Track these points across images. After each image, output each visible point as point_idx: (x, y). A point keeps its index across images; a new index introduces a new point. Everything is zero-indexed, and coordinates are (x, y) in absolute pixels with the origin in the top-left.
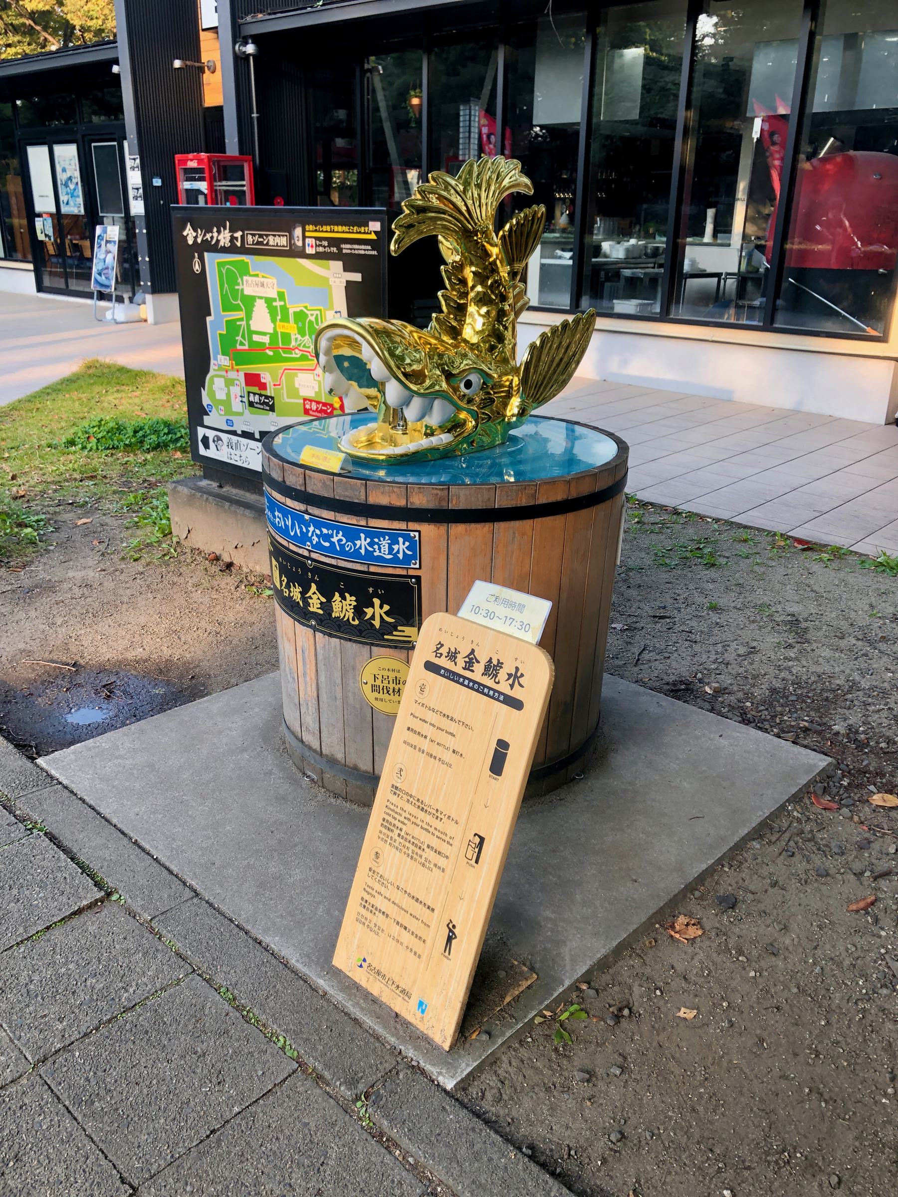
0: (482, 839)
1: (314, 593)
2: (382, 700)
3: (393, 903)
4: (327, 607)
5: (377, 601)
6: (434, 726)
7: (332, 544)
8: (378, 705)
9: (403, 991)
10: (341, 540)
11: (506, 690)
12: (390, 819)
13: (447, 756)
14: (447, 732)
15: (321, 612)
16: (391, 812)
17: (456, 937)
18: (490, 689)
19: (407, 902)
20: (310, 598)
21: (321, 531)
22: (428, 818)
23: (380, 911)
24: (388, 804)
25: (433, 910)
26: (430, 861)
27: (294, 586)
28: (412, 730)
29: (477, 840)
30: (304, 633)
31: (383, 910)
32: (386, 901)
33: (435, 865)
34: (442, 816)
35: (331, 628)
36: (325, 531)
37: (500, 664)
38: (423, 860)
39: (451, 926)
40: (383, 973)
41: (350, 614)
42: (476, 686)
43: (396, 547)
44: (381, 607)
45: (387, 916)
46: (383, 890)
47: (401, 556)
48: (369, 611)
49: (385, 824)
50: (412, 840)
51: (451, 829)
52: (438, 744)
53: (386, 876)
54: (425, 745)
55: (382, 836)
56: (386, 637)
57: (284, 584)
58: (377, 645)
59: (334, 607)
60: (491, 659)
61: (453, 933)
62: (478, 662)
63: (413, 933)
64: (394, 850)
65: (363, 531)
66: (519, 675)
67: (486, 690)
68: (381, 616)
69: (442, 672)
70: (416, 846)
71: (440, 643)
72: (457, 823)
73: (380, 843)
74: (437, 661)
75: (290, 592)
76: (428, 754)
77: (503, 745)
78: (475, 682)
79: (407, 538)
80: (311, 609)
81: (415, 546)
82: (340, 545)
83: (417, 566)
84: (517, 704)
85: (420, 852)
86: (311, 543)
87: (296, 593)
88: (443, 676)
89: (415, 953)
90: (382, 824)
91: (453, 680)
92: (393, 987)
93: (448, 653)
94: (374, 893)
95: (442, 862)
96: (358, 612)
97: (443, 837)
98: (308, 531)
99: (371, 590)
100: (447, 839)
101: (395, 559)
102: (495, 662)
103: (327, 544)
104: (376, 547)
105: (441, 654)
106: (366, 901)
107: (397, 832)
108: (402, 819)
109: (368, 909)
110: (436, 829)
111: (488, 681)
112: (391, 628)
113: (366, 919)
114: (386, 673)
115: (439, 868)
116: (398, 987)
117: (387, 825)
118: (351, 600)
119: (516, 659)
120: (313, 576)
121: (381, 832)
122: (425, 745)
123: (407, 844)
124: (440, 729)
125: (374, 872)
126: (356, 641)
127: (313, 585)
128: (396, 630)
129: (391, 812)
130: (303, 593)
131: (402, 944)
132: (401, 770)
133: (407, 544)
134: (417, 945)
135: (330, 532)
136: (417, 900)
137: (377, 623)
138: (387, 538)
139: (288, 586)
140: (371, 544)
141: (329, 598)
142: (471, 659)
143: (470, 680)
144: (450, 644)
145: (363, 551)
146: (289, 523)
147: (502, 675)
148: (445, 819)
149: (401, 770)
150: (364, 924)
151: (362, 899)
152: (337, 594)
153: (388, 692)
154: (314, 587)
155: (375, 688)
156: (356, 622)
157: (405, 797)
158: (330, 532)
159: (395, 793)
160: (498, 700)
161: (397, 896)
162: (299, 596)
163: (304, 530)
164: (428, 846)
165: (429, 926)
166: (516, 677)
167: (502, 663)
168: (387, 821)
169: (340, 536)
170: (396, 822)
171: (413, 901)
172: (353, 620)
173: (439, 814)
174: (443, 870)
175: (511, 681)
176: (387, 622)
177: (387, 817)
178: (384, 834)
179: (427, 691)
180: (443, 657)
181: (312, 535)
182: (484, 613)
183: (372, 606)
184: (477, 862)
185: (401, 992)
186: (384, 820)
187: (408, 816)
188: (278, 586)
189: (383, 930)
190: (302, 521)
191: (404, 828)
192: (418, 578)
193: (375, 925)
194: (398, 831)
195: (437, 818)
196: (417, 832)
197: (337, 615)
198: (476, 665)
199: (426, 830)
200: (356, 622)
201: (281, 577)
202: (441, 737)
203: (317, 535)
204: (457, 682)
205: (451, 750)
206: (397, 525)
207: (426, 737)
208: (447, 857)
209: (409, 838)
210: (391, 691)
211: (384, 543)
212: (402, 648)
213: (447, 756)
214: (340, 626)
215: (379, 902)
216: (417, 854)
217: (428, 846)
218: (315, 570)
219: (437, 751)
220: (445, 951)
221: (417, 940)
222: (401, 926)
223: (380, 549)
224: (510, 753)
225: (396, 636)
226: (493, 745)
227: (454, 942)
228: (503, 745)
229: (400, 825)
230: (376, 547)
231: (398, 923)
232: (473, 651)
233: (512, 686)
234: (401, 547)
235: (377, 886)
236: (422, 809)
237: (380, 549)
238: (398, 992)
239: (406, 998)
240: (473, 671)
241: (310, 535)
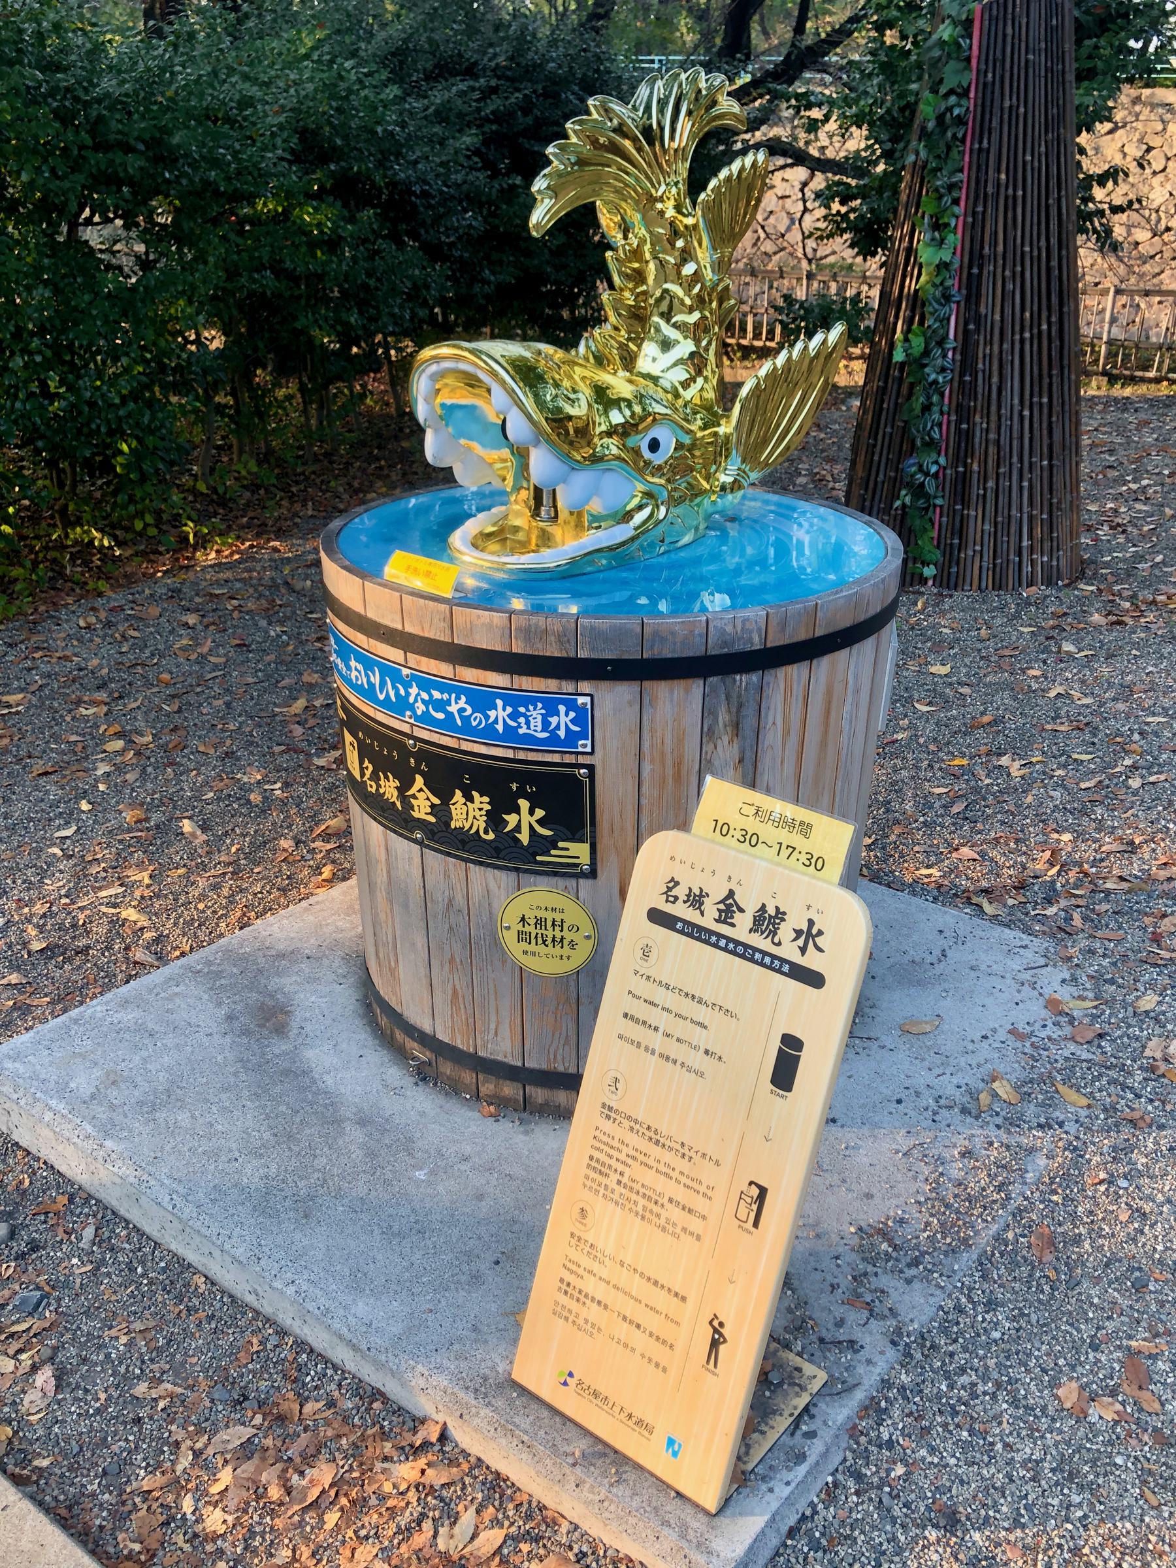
0: (763, 1191)
1: (421, 790)
2: (533, 954)
3: (615, 1287)
4: (442, 812)
5: (524, 804)
6: (668, 1011)
7: (450, 715)
8: (530, 962)
9: (639, 1423)
10: (464, 710)
11: (795, 957)
12: (602, 1157)
13: (697, 1060)
14: (692, 1021)
15: (432, 819)
16: (602, 1147)
17: (725, 1341)
18: (764, 953)
19: (637, 1285)
20: (414, 797)
21: (431, 696)
22: (668, 1157)
23: (593, 1299)
24: (597, 1133)
25: (684, 1299)
26: (674, 1224)
27: (387, 778)
28: (632, 1017)
29: (755, 1192)
30: (405, 850)
31: (598, 1298)
32: (603, 1284)
33: (684, 1230)
34: (692, 1154)
35: (451, 845)
36: (437, 695)
37: (780, 915)
38: (662, 1221)
39: (716, 1323)
40: (605, 1394)
41: (481, 824)
42: (740, 949)
43: (554, 720)
44: (531, 813)
45: (606, 1307)
46: (595, 1267)
47: (562, 733)
48: (512, 819)
49: (594, 1164)
50: (642, 1190)
51: (707, 1173)
52: (678, 1040)
53: (600, 1246)
54: (656, 1041)
55: (589, 1183)
56: (539, 858)
57: (368, 773)
58: (526, 871)
59: (454, 812)
60: (764, 905)
61: (721, 1335)
62: (741, 910)
63: (651, 1334)
64: (611, 1206)
65: (501, 696)
66: (814, 931)
67: (758, 956)
68: (531, 826)
69: (679, 925)
70: (649, 1199)
71: (672, 880)
72: (717, 1163)
73: (588, 1195)
74: (669, 908)
75: (379, 786)
76: (661, 1055)
77: (791, 1043)
78: (737, 943)
79: (571, 705)
80: (416, 814)
81: (584, 718)
82: (461, 717)
83: (589, 749)
84: (815, 980)
85: (656, 1209)
86: (414, 712)
87: (389, 788)
88: (681, 932)
89: (657, 1365)
90: (589, 1166)
91: (699, 939)
92: (623, 1416)
93: (689, 896)
94: (580, 1271)
95: (695, 1225)
96: (494, 819)
97: (689, 1182)
98: (408, 694)
99: (514, 786)
100: (702, 1189)
101: (554, 739)
102: (771, 911)
103: (440, 716)
104: (522, 720)
105: (676, 898)
106: (568, 1284)
107: (615, 1177)
108: (623, 1157)
109: (572, 1296)
110: (682, 1173)
111: (759, 941)
112: (540, 845)
113: (570, 1311)
114: (541, 914)
115: (691, 1234)
116: (630, 1416)
117: (598, 1167)
118: (481, 802)
119: (809, 907)
120: (418, 764)
121: (587, 1177)
122: (656, 1041)
123: (634, 1197)
124: (681, 1016)
125: (579, 1239)
126: (456, 857)
127: (418, 777)
128: (556, 847)
129: (602, 1147)
130: (402, 790)
131: (633, 1350)
132: (616, 1080)
133: (572, 715)
134: (657, 1352)
135: (446, 696)
136: (656, 1283)
137: (524, 837)
138: (540, 705)
139: (375, 777)
140: (514, 716)
141: (446, 797)
142: (729, 906)
143: (729, 940)
144: (689, 881)
145: (500, 727)
146: (376, 679)
147: (785, 932)
148: (697, 1159)
149: (616, 1080)
150: (567, 1319)
151: (562, 1280)
152: (458, 793)
153: (544, 942)
154: (419, 781)
155: (522, 937)
156: (491, 836)
157: (626, 1123)
158: (446, 696)
159: (608, 1117)
160: (779, 971)
161: (623, 1278)
162: (396, 793)
163: (402, 692)
164: (671, 1200)
165: (677, 1323)
166: (809, 934)
167: (784, 913)
168: (598, 1160)
169: (462, 703)
170: (613, 1162)
171: (650, 1285)
172: (486, 832)
173: (686, 1151)
174: (698, 1238)
175: (801, 942)
176: (541, 836)
177: (596, 1154)
178: (593, 1180)
179: (653, 956)
180: (680, 901)
181: (416, 701)
182: (738, 834)
183: (518, 812)
184: (756, 1224)
185: (637, 1423)
186: (591, 1158)
187: (633, 1153)
188: (357, 775)
189: (599, 1329)
190: (396, 677)
191: (627, 1171)
192: (591, 768)
193: (586, 1321)
194: (618, 1176)
195: (683, 1156)
196: (648, 1177)
197: (459, 825)
198: (737, 915)
199: (666, 1175)
200: (491, 836)
201: (361, 762)
202: (681, 1029)
203: (423, 701)
204: (707, 942)
205: (702, 1050)
206: (552, 684)
207: (656, 1029)
208: (704, 1218)
209: (637, 1187)
210: (549, 940)
211: (534, 713)
212: (564, 875)
213: (697, 1060)
214: (463, 842)
215: (590, 1285)
216: (651, 1211)
217: (671, 1200)
218: (421, 755)
219: (674, 1050)
220: (708, 1361)
221: (658, 1345)
222: (631, 1322)
223: (528, 723)
224: (805, 1056)
225: (556, 856)
226: (775, 1044)
227: (722, 1348)
228: (791, 1043)
229: (620, 1167)
230: (522, 720)
231: (625, 1318)
232: (731, 894)
233: (803, 950)
234: (563, 720)
235: (586, 1262)
236: (657, 1143)
237: (528, 723)
238: (630, 1423)
239: (646, 1433)
240: (733, 925)
241: (411, 700)
